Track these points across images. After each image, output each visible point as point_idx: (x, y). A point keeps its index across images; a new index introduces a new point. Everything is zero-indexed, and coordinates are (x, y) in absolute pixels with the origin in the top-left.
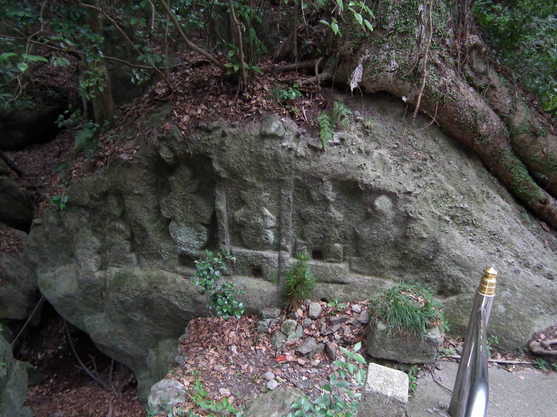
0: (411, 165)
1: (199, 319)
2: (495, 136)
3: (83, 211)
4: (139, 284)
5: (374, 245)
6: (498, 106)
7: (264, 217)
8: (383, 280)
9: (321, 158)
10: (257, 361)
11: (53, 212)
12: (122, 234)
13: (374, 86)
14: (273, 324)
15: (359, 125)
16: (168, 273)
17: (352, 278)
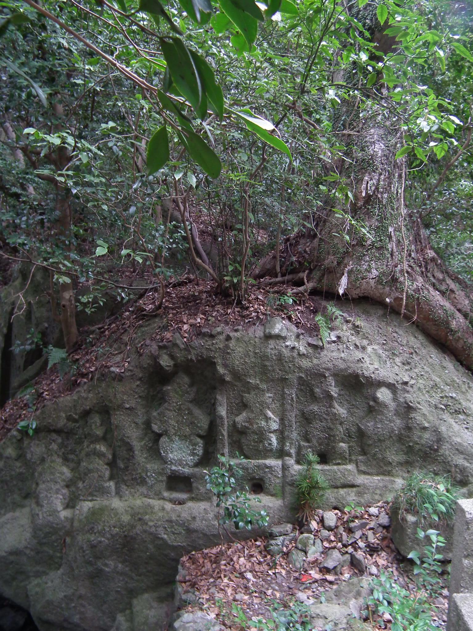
0: (401, 358)
1: (193, 553)
2: (463, 332)
3: (54, 436)
4: (119, 518)
5: (380, 440)
6: (459, 306)
7: (267, 419)
8: (392, 479)
9: (322, 355)
10: (280, 585)
11: (12, 443)
12: (103, 458)
13: (357, 291)
14: (287, 542)
15: (350, 325)
16: (153, 501)
17: (361, 479)
